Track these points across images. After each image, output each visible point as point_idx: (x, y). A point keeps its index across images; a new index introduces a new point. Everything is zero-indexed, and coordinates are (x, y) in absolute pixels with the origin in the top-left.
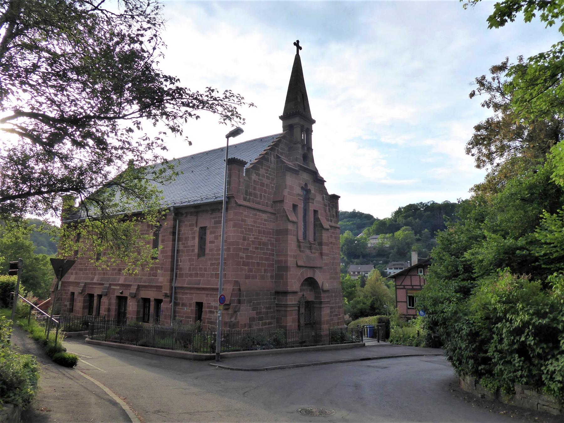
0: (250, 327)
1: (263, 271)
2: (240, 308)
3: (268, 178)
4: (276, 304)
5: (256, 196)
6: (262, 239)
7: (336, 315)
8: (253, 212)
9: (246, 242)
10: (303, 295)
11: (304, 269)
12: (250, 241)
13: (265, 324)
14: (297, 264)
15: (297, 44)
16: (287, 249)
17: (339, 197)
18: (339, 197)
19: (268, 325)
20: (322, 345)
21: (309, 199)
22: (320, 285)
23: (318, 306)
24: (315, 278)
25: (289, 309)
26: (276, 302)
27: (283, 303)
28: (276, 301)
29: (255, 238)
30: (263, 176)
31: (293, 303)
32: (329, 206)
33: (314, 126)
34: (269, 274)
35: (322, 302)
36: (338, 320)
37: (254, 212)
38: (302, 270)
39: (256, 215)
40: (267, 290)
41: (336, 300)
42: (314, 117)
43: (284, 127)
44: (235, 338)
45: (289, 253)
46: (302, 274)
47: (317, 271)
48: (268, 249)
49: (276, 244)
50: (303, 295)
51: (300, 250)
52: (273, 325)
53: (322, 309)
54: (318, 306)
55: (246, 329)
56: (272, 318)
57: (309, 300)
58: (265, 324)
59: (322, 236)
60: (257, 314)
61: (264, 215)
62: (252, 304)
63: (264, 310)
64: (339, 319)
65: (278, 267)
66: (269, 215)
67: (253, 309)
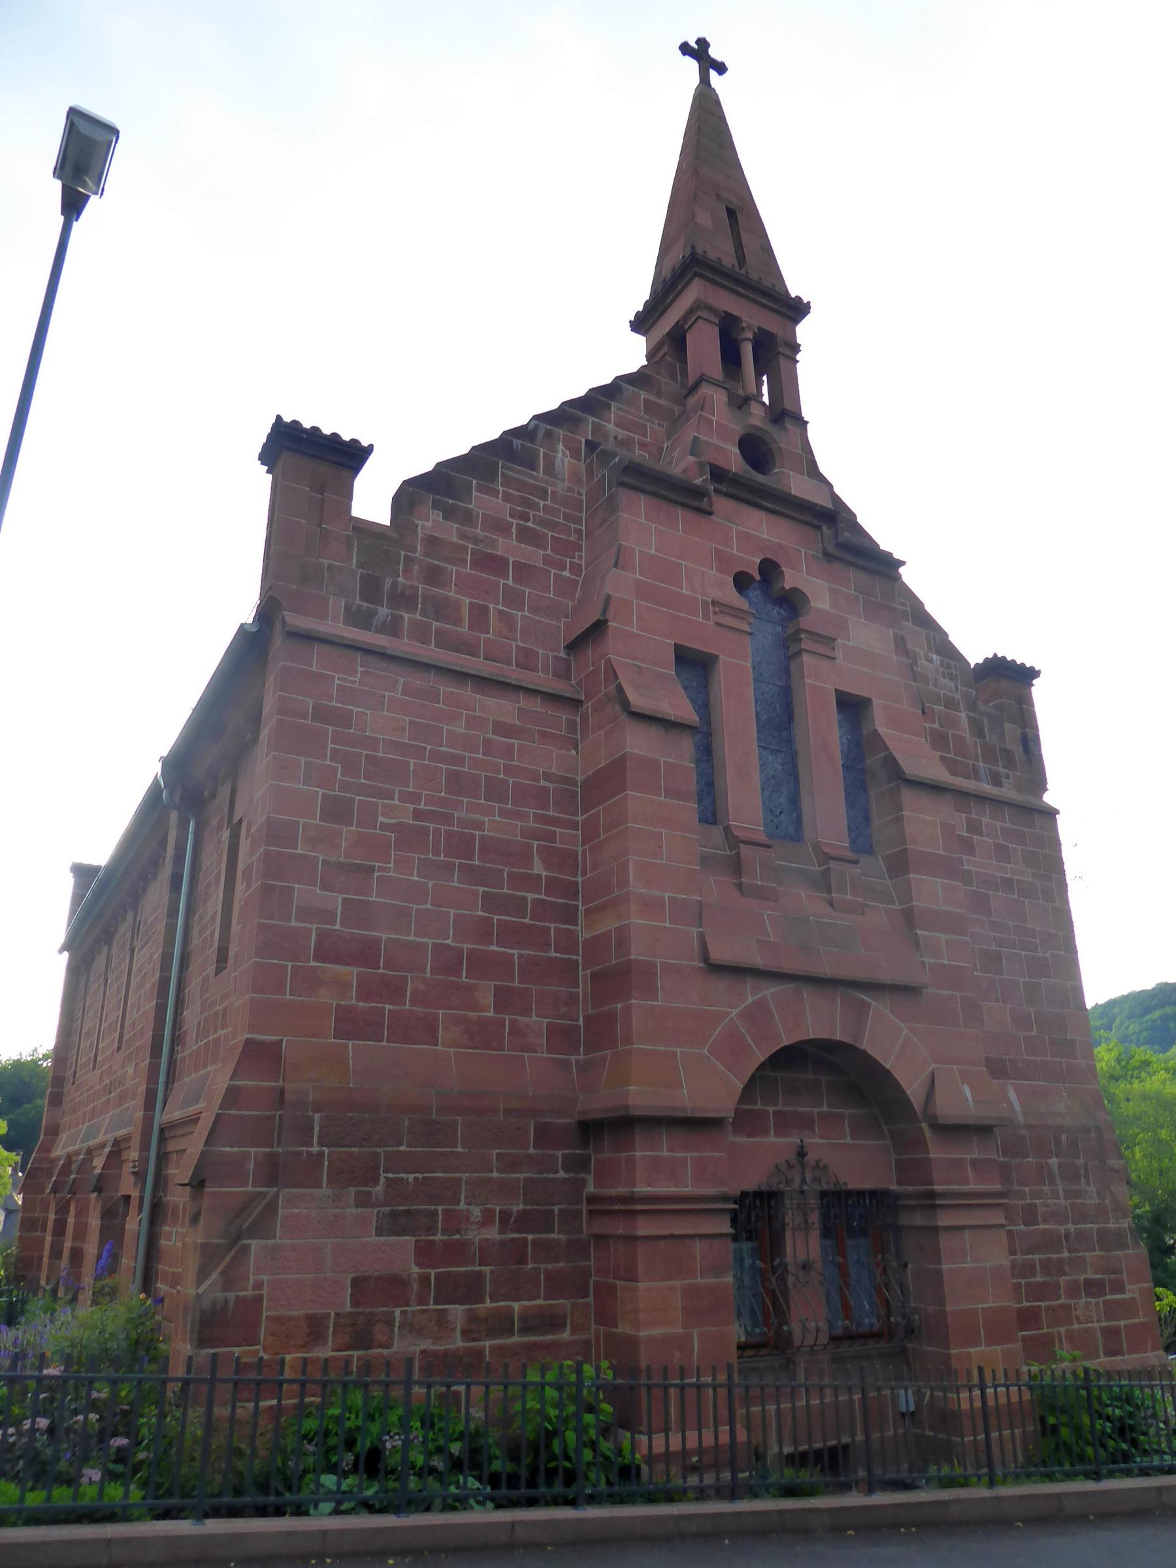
0: (361, 1335)
1: (490, 999)
2: (271, 1208)
3: (526, 535)
4: (592, 1199)
5: (442, 610)
6: (480, 826)
7: (1093, 1288)
8: (404, 678)
9: (348, 832)
10: (801, 1153)
11: (771, 991)
12: (384, 827)
13: (501, 1324)
14: (705, 957)
15: (698, 51)
16: (624, 868)
17: (1032, 674)
18: (1032, 674)
19: (526, 1330)
20: (947, 1483)
21: (795, 637)
22: (914, 1091)
23: (918, 1220)
24: (865, 1045)
25: (644, 1228)
26: (590, 1188)
27: (613, 1192)
28: (590, 1180)
29: (418, 815)
30: (501, 528)
31: (688, 1189)
32: (972, 706)
33: (804, 331)
34: (537, 1022)
35: (932, 1195)
36: (1109, 1316)
37: (420, 681)
38: (751, 994)
39: (433, 696)
40: (508, 1112)
41: (1079, 1194)
42: (795, 287)
43: (900, 576)
44: (221, 1412)
45: (636, 886)
46: (757, 1015)
47: (879, 1006)
48: (533, 882)
49: (584, 852)
50: (801, 1153)
51: (740, 887)
52: (566, 1336)
53: (946, 1242)
54: (918, 1220)
55: (325, 1352)
56: (557, 1285)
57: (853, 1185)
58: (501, 1324)
59: (899, 820)
60: (425, 1253)
61: (490, 701)
62: (379, 1189)
63: (493, 1234)
64: (1112, 1311)
65: (595, 977)
66: (537, 706)
67: (395, 1224)
